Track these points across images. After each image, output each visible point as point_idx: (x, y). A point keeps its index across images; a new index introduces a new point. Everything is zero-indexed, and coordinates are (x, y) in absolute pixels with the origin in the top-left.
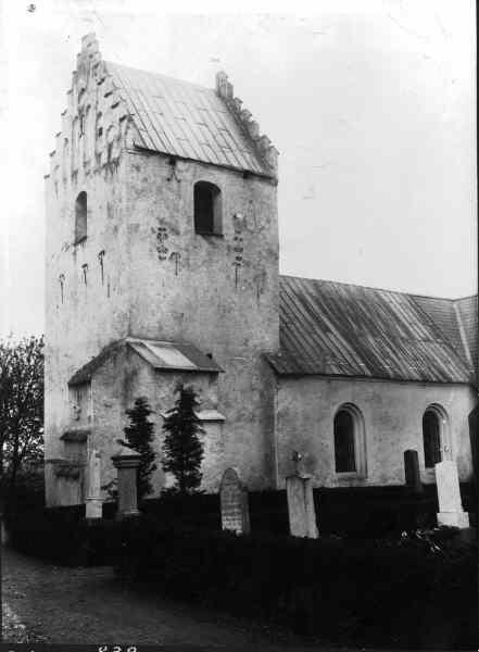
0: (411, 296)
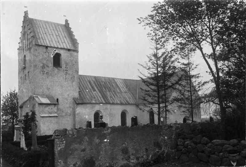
0: (124, 79)
